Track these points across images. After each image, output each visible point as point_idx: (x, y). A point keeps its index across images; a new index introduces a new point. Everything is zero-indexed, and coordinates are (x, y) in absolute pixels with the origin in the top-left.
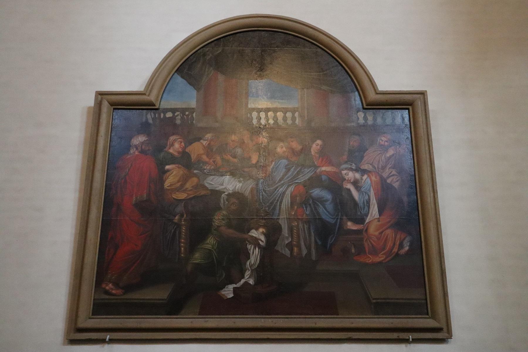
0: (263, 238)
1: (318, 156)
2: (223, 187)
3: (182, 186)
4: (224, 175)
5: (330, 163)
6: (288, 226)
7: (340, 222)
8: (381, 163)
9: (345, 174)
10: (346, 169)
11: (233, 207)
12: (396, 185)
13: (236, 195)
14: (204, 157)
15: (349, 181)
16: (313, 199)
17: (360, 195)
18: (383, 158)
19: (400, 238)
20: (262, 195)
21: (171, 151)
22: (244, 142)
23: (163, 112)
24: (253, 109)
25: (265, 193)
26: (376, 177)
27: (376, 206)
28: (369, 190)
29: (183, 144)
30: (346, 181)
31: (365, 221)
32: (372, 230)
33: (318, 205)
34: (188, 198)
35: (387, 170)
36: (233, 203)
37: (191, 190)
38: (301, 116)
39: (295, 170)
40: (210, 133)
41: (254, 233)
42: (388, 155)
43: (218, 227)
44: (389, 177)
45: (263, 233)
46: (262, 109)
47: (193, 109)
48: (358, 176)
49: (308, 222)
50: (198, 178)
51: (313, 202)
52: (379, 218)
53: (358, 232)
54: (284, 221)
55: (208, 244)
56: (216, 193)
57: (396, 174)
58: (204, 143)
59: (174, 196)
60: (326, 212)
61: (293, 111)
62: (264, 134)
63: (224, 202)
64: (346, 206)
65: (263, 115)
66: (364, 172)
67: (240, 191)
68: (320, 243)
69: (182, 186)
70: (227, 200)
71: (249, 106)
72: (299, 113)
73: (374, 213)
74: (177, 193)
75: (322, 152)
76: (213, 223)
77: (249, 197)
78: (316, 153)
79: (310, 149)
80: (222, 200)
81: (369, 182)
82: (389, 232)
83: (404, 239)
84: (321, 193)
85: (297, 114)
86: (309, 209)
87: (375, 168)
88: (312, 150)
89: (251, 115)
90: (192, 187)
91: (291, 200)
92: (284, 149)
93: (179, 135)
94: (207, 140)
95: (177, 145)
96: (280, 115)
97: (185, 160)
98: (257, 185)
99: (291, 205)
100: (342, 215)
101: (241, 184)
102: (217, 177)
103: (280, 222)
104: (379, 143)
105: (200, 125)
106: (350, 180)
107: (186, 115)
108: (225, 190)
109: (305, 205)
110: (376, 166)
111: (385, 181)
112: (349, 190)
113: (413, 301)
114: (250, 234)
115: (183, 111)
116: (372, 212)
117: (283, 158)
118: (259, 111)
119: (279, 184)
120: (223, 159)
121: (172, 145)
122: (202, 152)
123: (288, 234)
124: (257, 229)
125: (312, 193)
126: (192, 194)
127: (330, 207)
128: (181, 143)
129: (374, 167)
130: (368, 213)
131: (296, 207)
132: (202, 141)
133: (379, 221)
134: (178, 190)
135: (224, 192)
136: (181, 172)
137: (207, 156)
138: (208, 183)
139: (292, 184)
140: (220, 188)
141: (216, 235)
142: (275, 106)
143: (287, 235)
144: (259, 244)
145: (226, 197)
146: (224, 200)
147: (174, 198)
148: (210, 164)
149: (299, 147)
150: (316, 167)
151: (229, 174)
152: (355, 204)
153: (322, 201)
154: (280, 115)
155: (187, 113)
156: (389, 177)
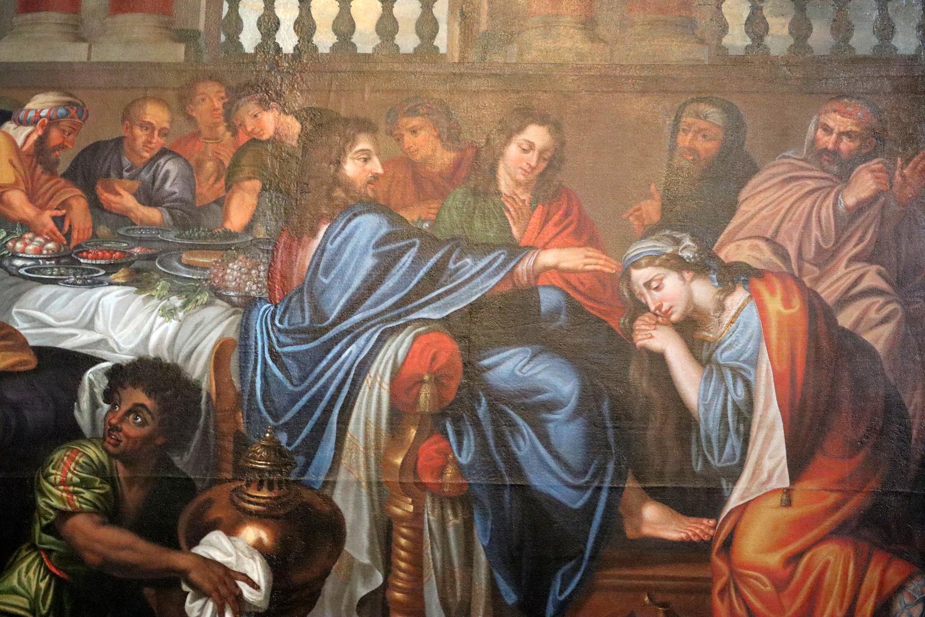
0: (256, 570)
1: (526, 197)
2: (96, 336)
5: (584, 234)
6: (374, 521)
7: (610, 507)
8: (815, 232)
9: (647, 285)
10: (652, 260)
11: (132, 429)
12: (879, 338)
15: (662, 317)
16: (497, 399)
17: (707, 379)
18: (827, 212)
19: (882, 583)
20: (264, 376)
25: (283, 367)
26: (787, 303)
27: (779, 435)
28: (754, 362)
30: (646, 317)
31: (723, 501)
32: (757, 545)
33: (513, 425)
35: (842, 270)
36: (136, 410)
41: (217, 547)
42: (850, 199)
43: (64, 515)
44: (846, 300)
45: (258, 546)
48: (703, 292)
49: (464, 501)
51: (492, 408)
52: (788, 491)
53: (692, 551)
54: (358, 495)
55: (14, 591)
57: (882, 284)
58: (21, 134)
60: (550, 463)
64: (638, 432)
66: (732, 275)
67: (167, 358)
68: (511, 598)
73: (768, 464)
75: (548, 180)
76: (41, 502)
77: (204, 386)
78: (518, 184)
79: (493, 170)
81: (755, 321)
82: (833, 557)
83: (900, 588)
84: (528, 371)
86: (470, 442)
87: (785, 257)
88: (502, 172)
92: (375, 166)
94: (34, 123)
98: (245, 329)
100: (620, 475)
101: (172, 325)
103: (338, 498)
104: (814, 141)
106: (667, 314)
109: (457, 421)
110: (792, 250)
111: (831, 321)
112: (659, 359)
114: (200, 550)
116: (758, 464)
123: (371, 553)
124: (231, 531)
125: (489, 368)
127: (567, 433)
129: (780, 251)
130: (742, 465)
131: (413, 432)
133: (788, 503)
137: (32, 197)
138: (33, 320)
141: (49, 552)
143: (365, 560)
144: (239, 598)
145: (103, 384)
148: (37, 234)
149: (444, 158)
150: (516, 250)
152: (685, 421)
153: (535, 407)
156: (846, 300)
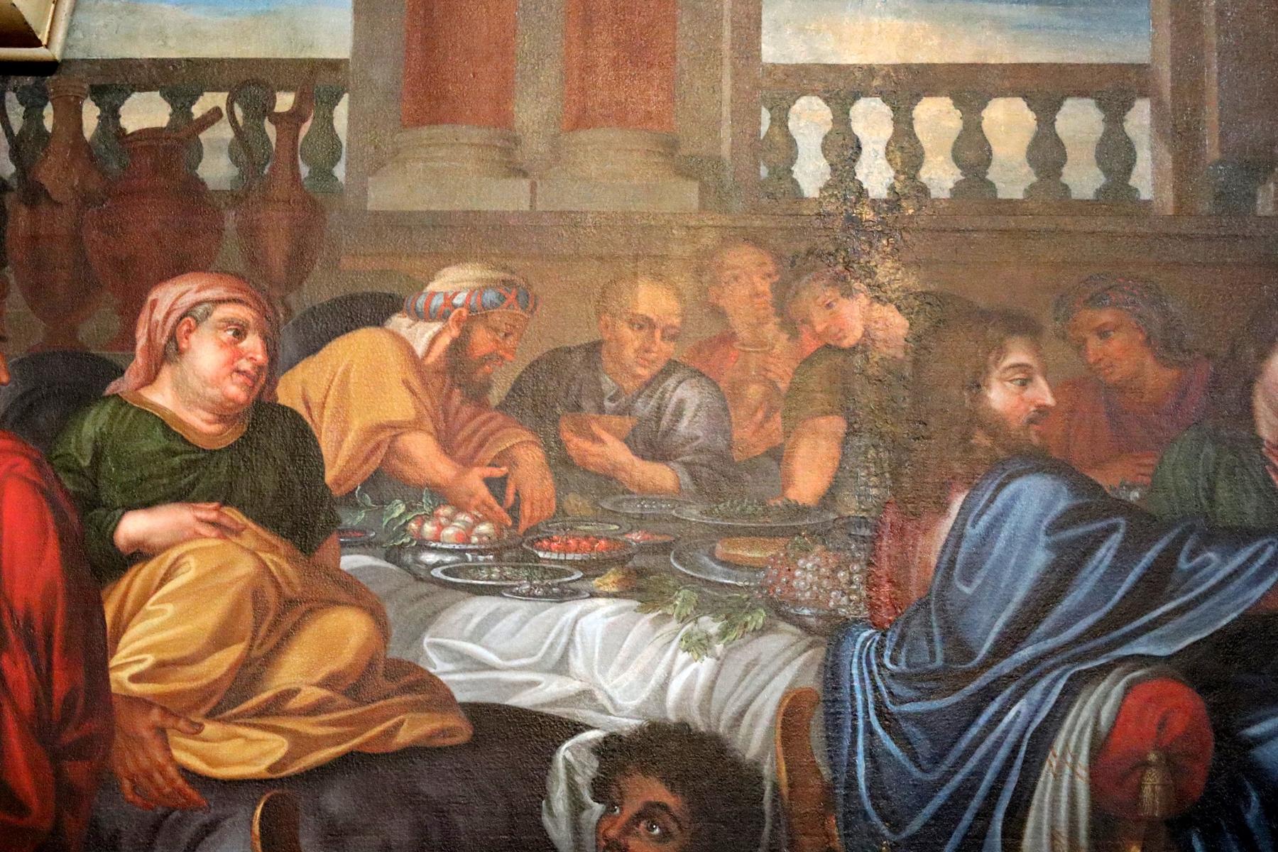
3: (247, 676)
4: (575, 594)
13: (668, 750)
14: (422, 450)
20: (871, 755)
21: (162, 396)
22: (727, 338)
23: (98, 93)
24: (800, 79)
29: (253, 343)
34: (292, 770)
36: (649, 813)
37: (313, 710)
38: (1180, 134)
39: (1124, 557)
40: (460, 258)
46: (870, 71)
47: (334, 65)
50: (375, 613)
56: (517, 737)
58: (421, 335)
59: (188, 753)
61: (1114, 88)
62: (885, 271)
63: (577, 806)
65: (872, 121)
67: (699, 723)
69: (247, 676)
70: (601, 789)
71: (771, 52)
72: (1157, 104)
74: (210, 728)
77: (767, 770)
80: (559, 800)
85: (1139, 120)
89: (781, 121)
90: (329, 682)
91: (1095, 808)
92: (1042, 393)
93: (222, 272)
94: (443, 317)
95: (206, 354)
96: (1009, 122)
97: (271, 474)
98: (832, 672)
99: (1093, 834)
101: (705, 666)
102: (524, 606)
105: (388, 193)
107: (278, 119)
108: (583, 714)
113: (1031, 729)
115: (250, 82)
117: (1038, 460)
118: (843, 87)
119: (1006, 666)
120: (562, 463)
121: (170, 352)
122: (399, 406)
125: (1260, 741)
126: (318, 743)
128: (240, 333)
132: (399, 322)
134: (234, 698)
135: (577, 728)
136: (245, 567)
137: (447, 444)
139: (1105, 670)
140: (542, 692)
142: (963, 50)
145: (589, 768)
146: (573, 788)
147: (185, 771)
148: (460, 508)
151: (609, 581)
154: (1009, 122)
155: (285, 101)
